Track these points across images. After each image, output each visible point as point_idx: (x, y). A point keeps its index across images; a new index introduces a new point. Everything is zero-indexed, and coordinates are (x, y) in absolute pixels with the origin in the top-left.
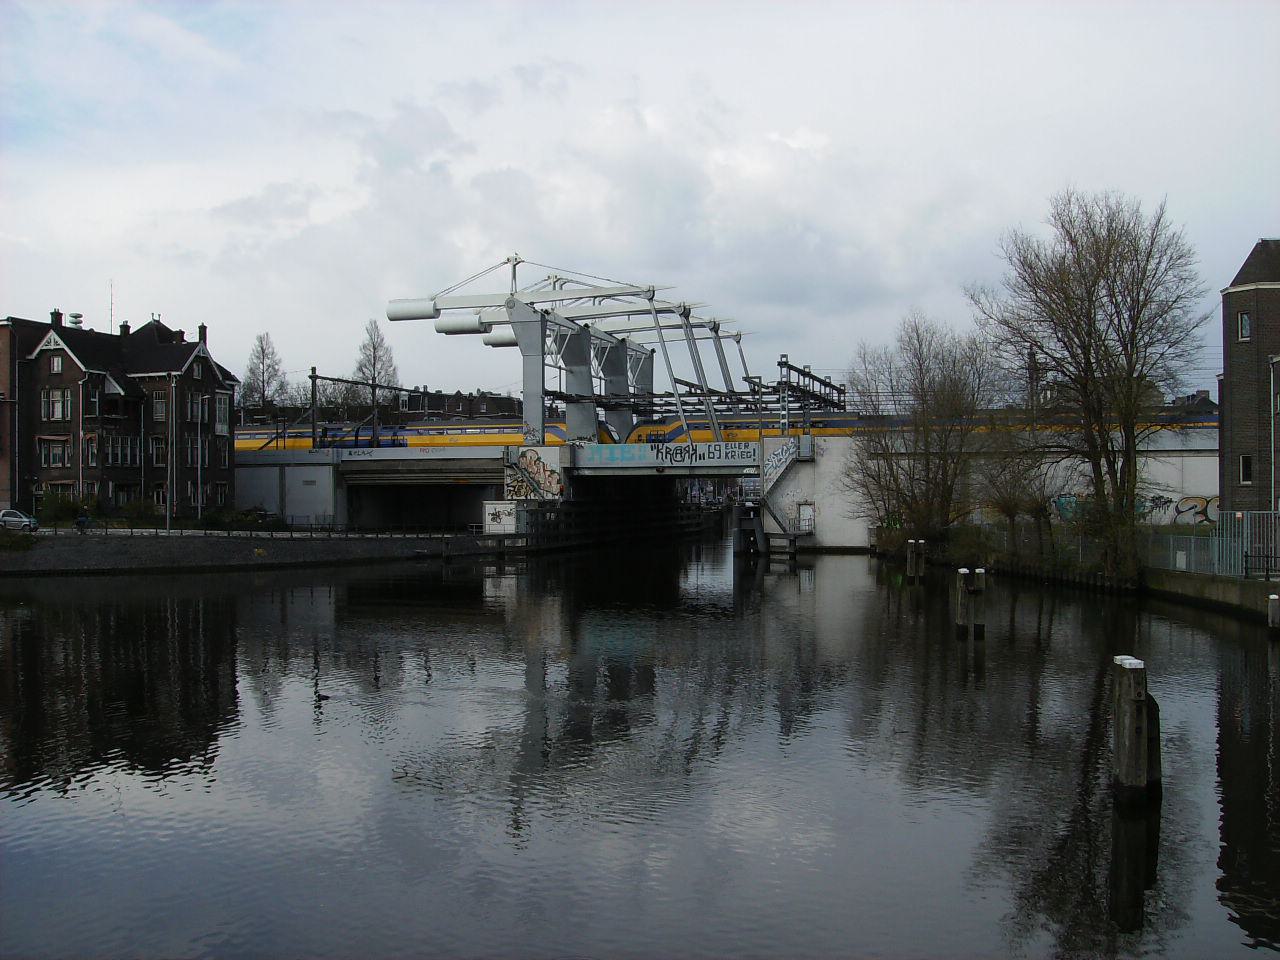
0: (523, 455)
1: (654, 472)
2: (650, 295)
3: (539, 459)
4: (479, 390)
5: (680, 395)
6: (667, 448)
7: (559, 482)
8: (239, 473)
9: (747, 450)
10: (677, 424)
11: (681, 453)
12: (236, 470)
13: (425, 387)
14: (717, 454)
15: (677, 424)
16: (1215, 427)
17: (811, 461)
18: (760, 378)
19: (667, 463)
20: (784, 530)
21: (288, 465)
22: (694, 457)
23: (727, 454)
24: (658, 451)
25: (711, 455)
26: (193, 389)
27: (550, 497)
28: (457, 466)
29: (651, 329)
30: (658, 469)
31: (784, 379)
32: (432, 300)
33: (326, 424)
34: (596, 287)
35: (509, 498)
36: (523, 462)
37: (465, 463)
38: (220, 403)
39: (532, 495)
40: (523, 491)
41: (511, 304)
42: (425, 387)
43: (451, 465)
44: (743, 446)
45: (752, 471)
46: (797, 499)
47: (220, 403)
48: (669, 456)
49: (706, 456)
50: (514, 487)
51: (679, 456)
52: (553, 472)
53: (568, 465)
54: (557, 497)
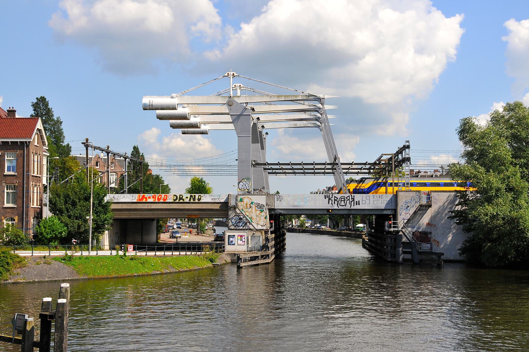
4: (37, 98)
6: (335, 197)
10: (69, 335)
11: (344, 201)
13: (51, 108)
14: (367, 201)
15: (69, 335)
16: (38, 350)
19: (336, 207)
22: (353, 203)
24: (329, 199)
25: (364, 202)
48: (336, 202)
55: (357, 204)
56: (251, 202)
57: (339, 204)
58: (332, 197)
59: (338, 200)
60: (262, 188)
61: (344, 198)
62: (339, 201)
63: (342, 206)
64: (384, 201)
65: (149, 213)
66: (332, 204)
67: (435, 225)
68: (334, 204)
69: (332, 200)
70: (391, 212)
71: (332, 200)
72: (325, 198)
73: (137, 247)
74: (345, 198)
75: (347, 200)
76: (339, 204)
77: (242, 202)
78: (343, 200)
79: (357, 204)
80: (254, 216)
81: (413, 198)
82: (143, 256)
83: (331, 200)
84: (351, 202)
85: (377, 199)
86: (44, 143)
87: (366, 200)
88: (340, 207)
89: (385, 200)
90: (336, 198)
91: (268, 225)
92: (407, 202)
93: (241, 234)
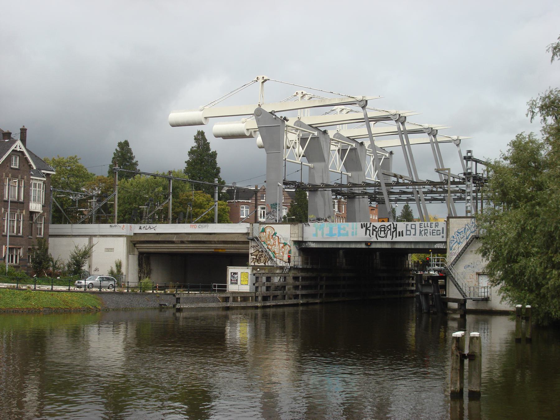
0: (264, 231)
1: (363, 246)
2: (364, 104)
3: (275, 234)
4: (137, 161)
6: (373, 226)
8: (51, 240)
11: (384, 231)
12: (50, 239)
14: (413, 231)
19: (374, 239)
21: (95, 236)
22: (395, 233)
23: (420, 232)
24: (367, 229)
25: (408, 233)
26: (10, 175)
28: (190, 238)
29: (440, 142)
30: (366, 243)
33: (309, 221)
34: (322, 99)
37: (221, 236)
39: (269, 262)
40: (262, 259)
41: (259, 113)
43: (211, 238)
44: (433, 225)
47: (35, 186)
48: (375, 233)
50: (256, 256)
52: (285, 244)
53: (296, 239)
56: (273, 232)
57: (378, 236)
58: (370, 227)
59: (377, 230)
60: (328, 217)
61: (384, 228)
62: (378, 232)
66: (370, 235)
68: (373, 234)
72: (362, 228)
74: (386, 228)
75: (388, 229)
77: (264, 233)
79: (399, 236)
83: (369, 230)
84: (393, 232)
85: (425, 228)
87: (412, 230)
88: (380, 239)
89: (435, 230)
92: (459, 231)
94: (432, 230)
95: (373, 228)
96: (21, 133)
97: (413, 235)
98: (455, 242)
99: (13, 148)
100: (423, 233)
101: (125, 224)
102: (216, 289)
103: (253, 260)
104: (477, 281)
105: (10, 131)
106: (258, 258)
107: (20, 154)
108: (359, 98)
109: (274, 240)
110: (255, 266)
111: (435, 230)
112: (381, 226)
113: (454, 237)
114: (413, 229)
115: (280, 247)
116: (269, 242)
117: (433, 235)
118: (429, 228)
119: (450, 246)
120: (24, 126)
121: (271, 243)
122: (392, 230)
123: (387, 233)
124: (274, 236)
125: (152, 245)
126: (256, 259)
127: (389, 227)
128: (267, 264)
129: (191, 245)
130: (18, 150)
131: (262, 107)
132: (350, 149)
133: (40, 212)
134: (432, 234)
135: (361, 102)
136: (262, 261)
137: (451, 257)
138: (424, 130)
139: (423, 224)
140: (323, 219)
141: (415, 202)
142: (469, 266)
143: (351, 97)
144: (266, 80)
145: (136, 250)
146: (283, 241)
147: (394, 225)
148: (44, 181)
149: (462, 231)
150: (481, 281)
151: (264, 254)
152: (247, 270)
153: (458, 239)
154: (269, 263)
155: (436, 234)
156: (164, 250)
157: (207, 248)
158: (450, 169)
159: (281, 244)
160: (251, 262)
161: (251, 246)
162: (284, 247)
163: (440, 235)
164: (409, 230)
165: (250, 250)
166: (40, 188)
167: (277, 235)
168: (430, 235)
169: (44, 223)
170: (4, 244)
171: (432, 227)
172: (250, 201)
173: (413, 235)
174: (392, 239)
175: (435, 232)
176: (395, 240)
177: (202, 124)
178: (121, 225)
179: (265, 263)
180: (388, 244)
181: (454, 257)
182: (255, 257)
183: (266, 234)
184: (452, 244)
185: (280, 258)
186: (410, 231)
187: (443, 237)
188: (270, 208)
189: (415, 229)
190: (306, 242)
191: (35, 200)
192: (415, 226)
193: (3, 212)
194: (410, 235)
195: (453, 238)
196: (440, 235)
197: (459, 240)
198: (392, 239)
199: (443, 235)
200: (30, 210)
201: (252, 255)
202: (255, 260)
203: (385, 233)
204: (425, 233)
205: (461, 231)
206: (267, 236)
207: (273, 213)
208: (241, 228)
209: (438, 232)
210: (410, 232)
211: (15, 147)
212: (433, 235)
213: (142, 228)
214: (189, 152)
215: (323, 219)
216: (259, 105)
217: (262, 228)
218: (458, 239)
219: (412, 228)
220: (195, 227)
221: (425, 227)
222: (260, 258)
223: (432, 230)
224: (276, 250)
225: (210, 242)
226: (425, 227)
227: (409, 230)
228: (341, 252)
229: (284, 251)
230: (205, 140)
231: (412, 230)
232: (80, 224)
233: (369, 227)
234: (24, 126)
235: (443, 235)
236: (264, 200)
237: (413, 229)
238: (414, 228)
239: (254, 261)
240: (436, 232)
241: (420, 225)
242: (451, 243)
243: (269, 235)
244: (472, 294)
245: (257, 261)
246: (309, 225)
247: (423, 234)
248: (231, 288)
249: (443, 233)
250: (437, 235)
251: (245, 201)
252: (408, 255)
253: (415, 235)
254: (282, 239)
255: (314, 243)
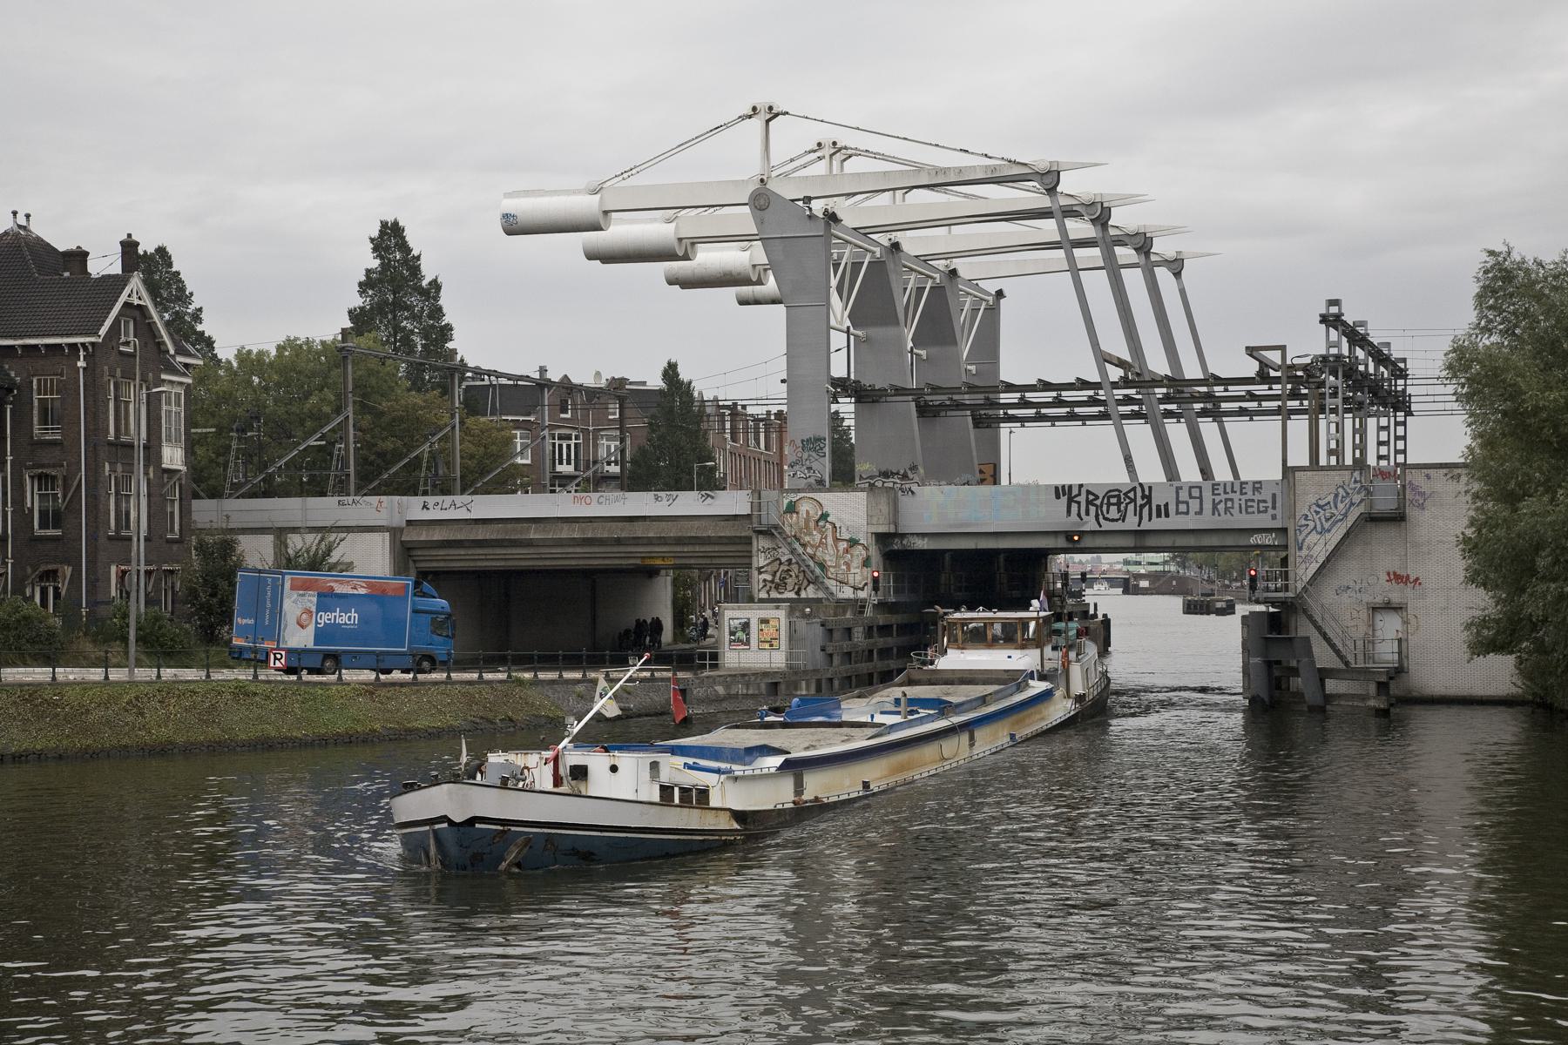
0: (792, 508)
2: (1049, 179)
3: (824, 516)
5: (1115, 385)
7: (866, 563)
9: (1257, 497)
11: (1118, 504)
14: (1194, 505)
17: (1397, 518)
18: (1283, 348)
19: (1090, 524)
20: (1347, 663)
21: (294, 530)
24: (1071, 500)
27: (847, 593)
28: (672, 531)
31: (1334, 351)
32: (595, 192)
33: (857, 479)
35: (763, 595)
36: (791, 524)
38: (169, 403)
41: (761, 200)
42: (543, 370)
43: (639, 531)
45: (1267, 539)
46: (1367, 598)
48: (1092, 509)
49: (1172, 508)
51: (1113, 509)
52: (853, 543)
53: (882, 529)
54: (862, 595)
55: (1159, 515)
56: (820, 513)
57: (1101, 517)
58: (1079, 494)
59: (1098, 502)
60: (911, 469)
61: (1118, 497)
62: (1102, 507)
63: (1113, 520)
64: (1249, 504)
65: (664, 550)
66: (1079, 515)
67: (1417, 579)
68: (1087, 513)
69: (1079, 503)
70: (1274, 539)
71: (1079, 503)
72: (1058, 497)
73: (611, 656)
74: (1122, 496)
75: (1128, 501)
76: (1101, 517)
77: (795, 515)
78: (1114, 500)
79: (1159, 515)
80: (830, 560)
81: (1340, 490)
82: (39, 685)
83: (1076, 502)
84: (1142, 507)
85: (1227, 496)
86: (162, 347)
87: (1187, 498)
88: (1107, 526)
89: (1253, 501)
90: (1091, 497)
91: (1492, 602)
92: (1321, 503)
93: (764, 614)
94: (1246, 501)
95: (1087, 498)
96: (124, 253)
97: (1196, 513)
98: (1309, 529)
99: (123, 298)
100: (1221, 507)
101: (383, 498)
102: (708, 662)
103: (765, 586)
104: (1369, 626)
105: (85, 248)
106: (777, 580)
107: (137, 313)
108: (1042, 166)
109: (822, 532)
110: (799, 600)
111: (1253, 501)
112: (1110, 491)
113: (1307, 516)
114: (1195, 498)
115: (838, 551)
116: (807, 539)
117: (1247, 512)
118: (1236, 497)
119: (1296, 540)
120: (129, 236)
121: (814, 540)
122: (1140, 501)
123: (1126, 510)
124: (821, 523)
125: (462, 552)
126: (772, 582)
127: (1131, 495)
128: (803, 595)
129: (578, 550)
130: (136, 302)
131: (771, 186)
132: (931, 288)
133: (180, 471)
134: (1246, 510)
135: (1044, 177)
136: (789, 587)
137: (1303, 572)
138: (1126, 240)
139: (561, 442)
140: (898, 474)
141: (1111, 422)
142: (1348, 588)
143: (1019, 163)
144: (777, 115)
145: (411, 564)
146: (847, 537)
147: (1143, 491)
148: (189, 385)
149: (1329, 503)
150: (1379, 625)
151: (795, 567)
152: (774, 611)
153: (1318, 523)
154: (810, 592)
155: (1255, 509)
156: (494, 564)
157: (623, 555)
158: (1285, 346)
159: (841, 543)
160: (759, 591)
161: (759, 550)
162: (850, 550)
163: (1266, 511)
164: (1183, 502)
165: (755, 559)
166: (179, 406)
167: (829, 519)
168: (1241, 512)
169: (181, 499)
170: (113, 562)
171: (1246, 493)
172: (532, 419)
173: (1196, 513)
174: (1139, 525)
175: (1252, 507)
176: (1146, 525)
177: (599, 228)
178: (374, 499)
179: (798, 593)
180: (1056, 537)
181: (1314, 567)
182: (769, 578)
183: (798, 518)
184: (1304, 534)
185: (840, 577)
186: (1187, 503)
187: (1274, 517)
188: (800, 449)
189: (1201, 498)
190: (903, 536)
191: (169, 440)
192: (1201, 492)
193: (107, 474)
194: (1187, 513)
195: (1306, 519)
196: (1266, 511)
197: (1321, 523)
198: (1139, 525)
199: (1274, 512)
200: (163, 466)
201: (760, 573)
202: (769, 584)
203: (1119, 511)
204: (1226, 509)
205: (1326, 501)
206: (802, 523)
207: (808, 462)
208: (732, 502)
209: (1261, 505)
210: (1188, 507)
211: (129, 296)
212: (1247, 512)
213: (430, 506)
214: (360, 284)
215: (898, 474)
216: (762, 180)
217: (786, 502)
218: (1318, 523)
219: (1191, 497)
220: (588, 500)
221: (1225, 493)
222: (784, 578)
223: (1246, 501)
224: (827, 558)
225: (636, 541)
226: (1225, 493)
227: (1183, 502)
228: (947, 557)
229: (852, 561)
230: (404, 247)
231: (1187, 498)
232: (238, 498)
233: (1076, 496)
234: (129, 236)
235: (1274, 512)
236: (568, 416)
237: (1195, 498)
238: (1198, 495)
239: (768, 588)
240: (1255, 505)
241: (1213, 489)
242: (1301, 532)
243: (807, 521)
244: (1360, 657)
245: (777, 588)
246: (913, 492)
247: (1222, 513)
248: (733, 658)
249: (1274, 508)
250: (1259, 512)
251: (521, 418)
252: (1046, 559)
253: (1200, 512)
254: (843, 530)
255: (926, 539)
